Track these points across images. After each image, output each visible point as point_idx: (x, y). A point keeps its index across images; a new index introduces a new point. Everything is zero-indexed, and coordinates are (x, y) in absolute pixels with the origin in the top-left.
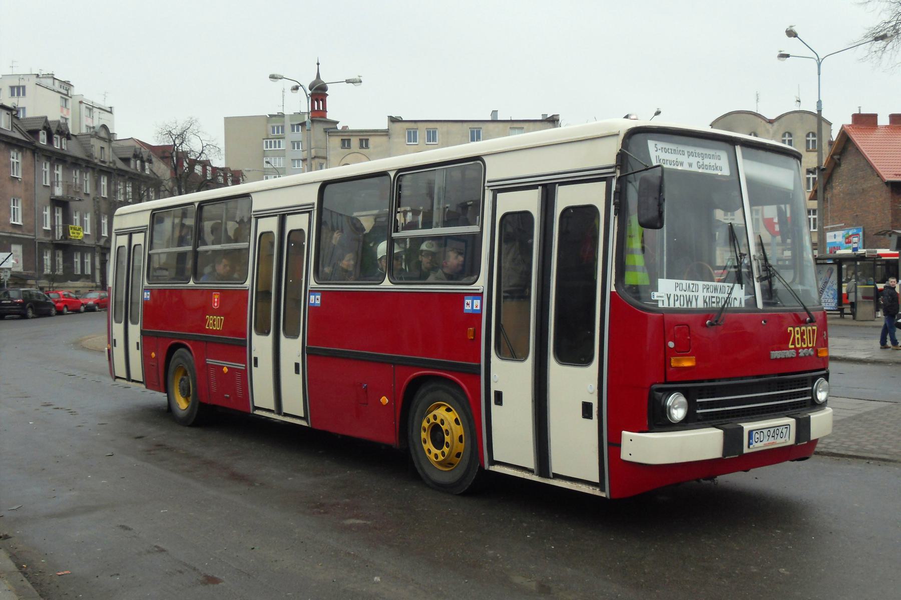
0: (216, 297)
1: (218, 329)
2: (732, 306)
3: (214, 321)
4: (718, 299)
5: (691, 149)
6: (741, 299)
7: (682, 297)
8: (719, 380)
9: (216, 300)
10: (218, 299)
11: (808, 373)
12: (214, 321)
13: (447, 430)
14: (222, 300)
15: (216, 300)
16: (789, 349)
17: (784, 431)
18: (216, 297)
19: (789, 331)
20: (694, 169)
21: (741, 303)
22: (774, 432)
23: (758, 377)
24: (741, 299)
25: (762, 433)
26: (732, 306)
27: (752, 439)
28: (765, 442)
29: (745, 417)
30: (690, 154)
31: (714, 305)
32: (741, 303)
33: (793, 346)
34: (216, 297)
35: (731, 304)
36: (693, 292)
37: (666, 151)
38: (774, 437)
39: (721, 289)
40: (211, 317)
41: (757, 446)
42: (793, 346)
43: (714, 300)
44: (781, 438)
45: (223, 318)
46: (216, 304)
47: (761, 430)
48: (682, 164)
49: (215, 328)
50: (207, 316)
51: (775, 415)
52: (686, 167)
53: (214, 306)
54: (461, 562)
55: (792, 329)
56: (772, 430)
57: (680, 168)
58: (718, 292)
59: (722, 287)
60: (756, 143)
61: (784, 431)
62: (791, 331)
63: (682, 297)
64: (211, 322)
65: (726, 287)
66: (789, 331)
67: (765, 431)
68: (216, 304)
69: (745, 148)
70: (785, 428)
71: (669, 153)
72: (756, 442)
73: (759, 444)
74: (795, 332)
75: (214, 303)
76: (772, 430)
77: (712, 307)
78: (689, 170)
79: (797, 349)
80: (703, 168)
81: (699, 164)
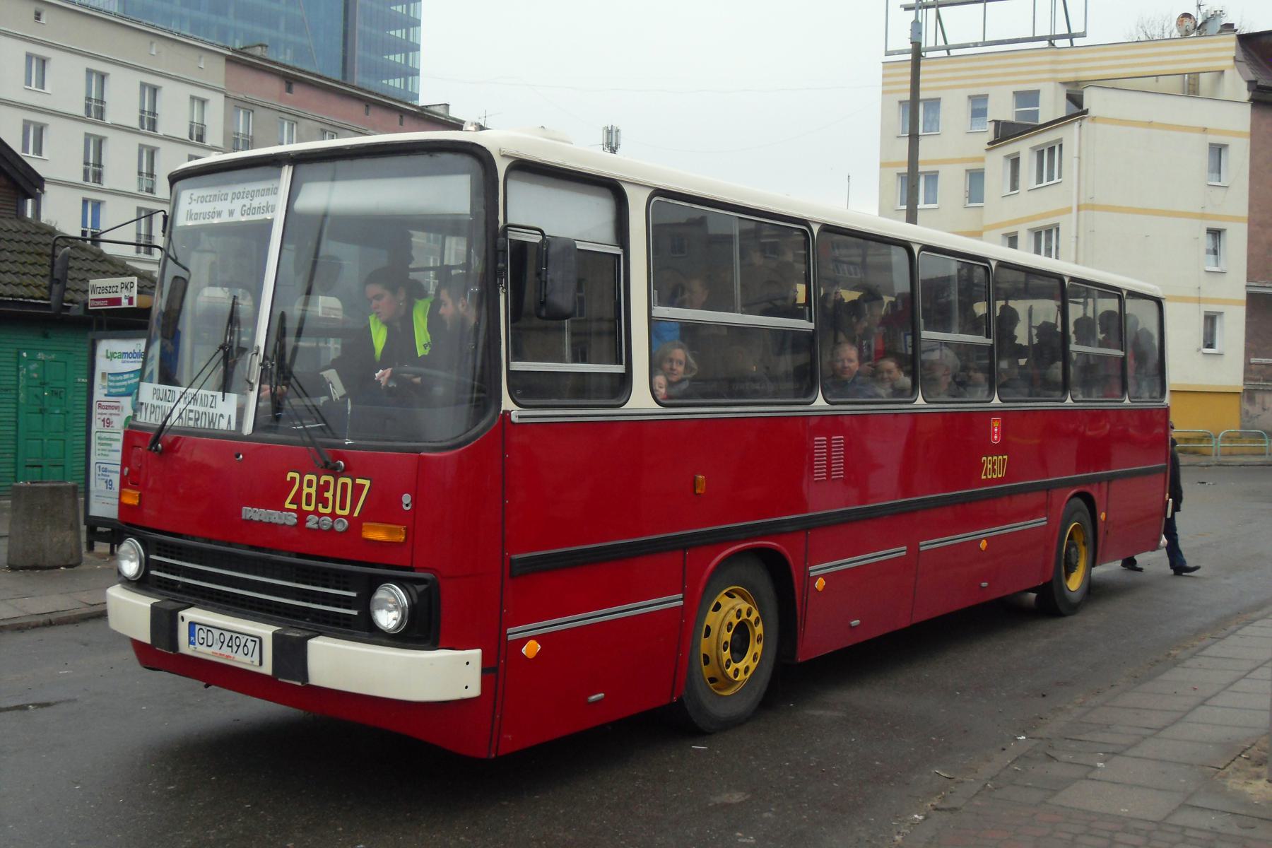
0: (996, 424)
1: (1000, 476)
2: (216, 427)
3: (994, 464)
4: (197, 414)
5: (239, 188)
6: (230, 416)
7: (204, 416)
8: (193, 538)
9: (996, 430)
10: (998, 428)
11: (407, 571)
12: (994, 464)
13: (708, 628)
14: (1004, 431)
15: (996, 430)
16: (283, 509)
17: (250, 644)
18: (996, 425)
19: (288, 479)
20: (238, 218)
21: (229, 422)
22: (231, 638)
23: (300, 556)
24: (230, 416)
25: (209, 633)
26: (216, 427)
27: (194, 636)
28: (215, 648)
29: (213, 603)
30: (236, 196)
31: (191, 423)
32: (229, 422)
33: (294, 507)
34: (996, 425)
35: (214, 424)
36: (212, 407)
37: (203, 200)
38: (231, 647)
39: (201, 399)
40: (990, 458)
41: (201, 651)
42: (294, 507)
43: (192, 415)
44: (246, 655)
45: (1005, 457)
46: (996, 437)
47: (210, 628)
48: (219, 214)
49: (995, 476)
50: (984, 458)
51: (264, 617)
52: (225, 218)
53: (993, 438)
54: (711, 839)
55: (297, 475)
56: (228, 635)
57: (216, 221)
58: (198, 404)
59: (203, 396)
60: (207, 167)
61: (250, 644)
62: (293, 479)
63: (204, 416)
64: (990, 466)
65: (209, 396)
66: (288, 479)
67: (216, 633)
68: (996, 437)
69: (1070, 103)
70: (252, 641)
71: (221, 200)
72: (202, 644)
73: (204, 648)
74: (308, 484)
75: (994, 435)
76: (228, 635)
77: (189, 427)
78: (230, 221)
79: (302, 515)
80: (248, 214)
81: (244, 208)
